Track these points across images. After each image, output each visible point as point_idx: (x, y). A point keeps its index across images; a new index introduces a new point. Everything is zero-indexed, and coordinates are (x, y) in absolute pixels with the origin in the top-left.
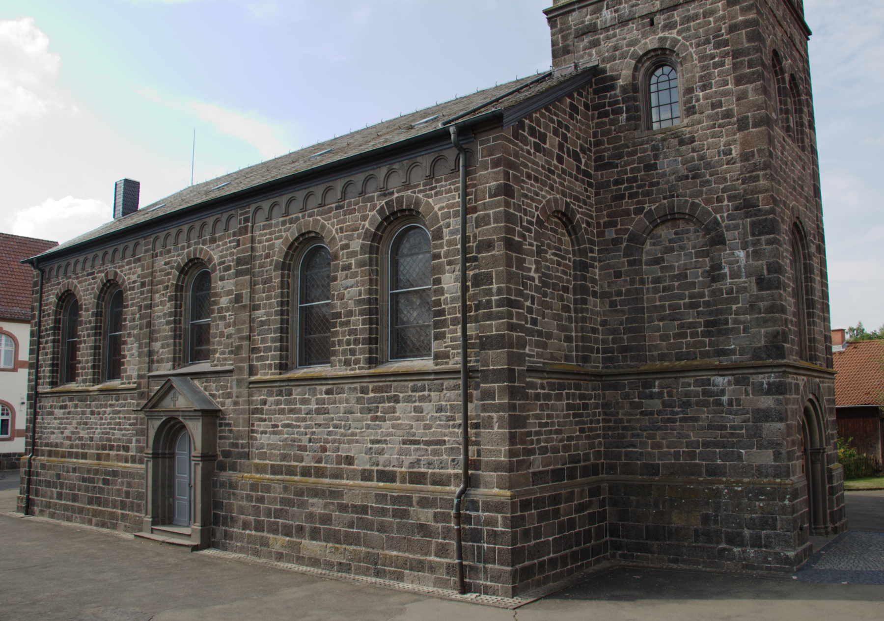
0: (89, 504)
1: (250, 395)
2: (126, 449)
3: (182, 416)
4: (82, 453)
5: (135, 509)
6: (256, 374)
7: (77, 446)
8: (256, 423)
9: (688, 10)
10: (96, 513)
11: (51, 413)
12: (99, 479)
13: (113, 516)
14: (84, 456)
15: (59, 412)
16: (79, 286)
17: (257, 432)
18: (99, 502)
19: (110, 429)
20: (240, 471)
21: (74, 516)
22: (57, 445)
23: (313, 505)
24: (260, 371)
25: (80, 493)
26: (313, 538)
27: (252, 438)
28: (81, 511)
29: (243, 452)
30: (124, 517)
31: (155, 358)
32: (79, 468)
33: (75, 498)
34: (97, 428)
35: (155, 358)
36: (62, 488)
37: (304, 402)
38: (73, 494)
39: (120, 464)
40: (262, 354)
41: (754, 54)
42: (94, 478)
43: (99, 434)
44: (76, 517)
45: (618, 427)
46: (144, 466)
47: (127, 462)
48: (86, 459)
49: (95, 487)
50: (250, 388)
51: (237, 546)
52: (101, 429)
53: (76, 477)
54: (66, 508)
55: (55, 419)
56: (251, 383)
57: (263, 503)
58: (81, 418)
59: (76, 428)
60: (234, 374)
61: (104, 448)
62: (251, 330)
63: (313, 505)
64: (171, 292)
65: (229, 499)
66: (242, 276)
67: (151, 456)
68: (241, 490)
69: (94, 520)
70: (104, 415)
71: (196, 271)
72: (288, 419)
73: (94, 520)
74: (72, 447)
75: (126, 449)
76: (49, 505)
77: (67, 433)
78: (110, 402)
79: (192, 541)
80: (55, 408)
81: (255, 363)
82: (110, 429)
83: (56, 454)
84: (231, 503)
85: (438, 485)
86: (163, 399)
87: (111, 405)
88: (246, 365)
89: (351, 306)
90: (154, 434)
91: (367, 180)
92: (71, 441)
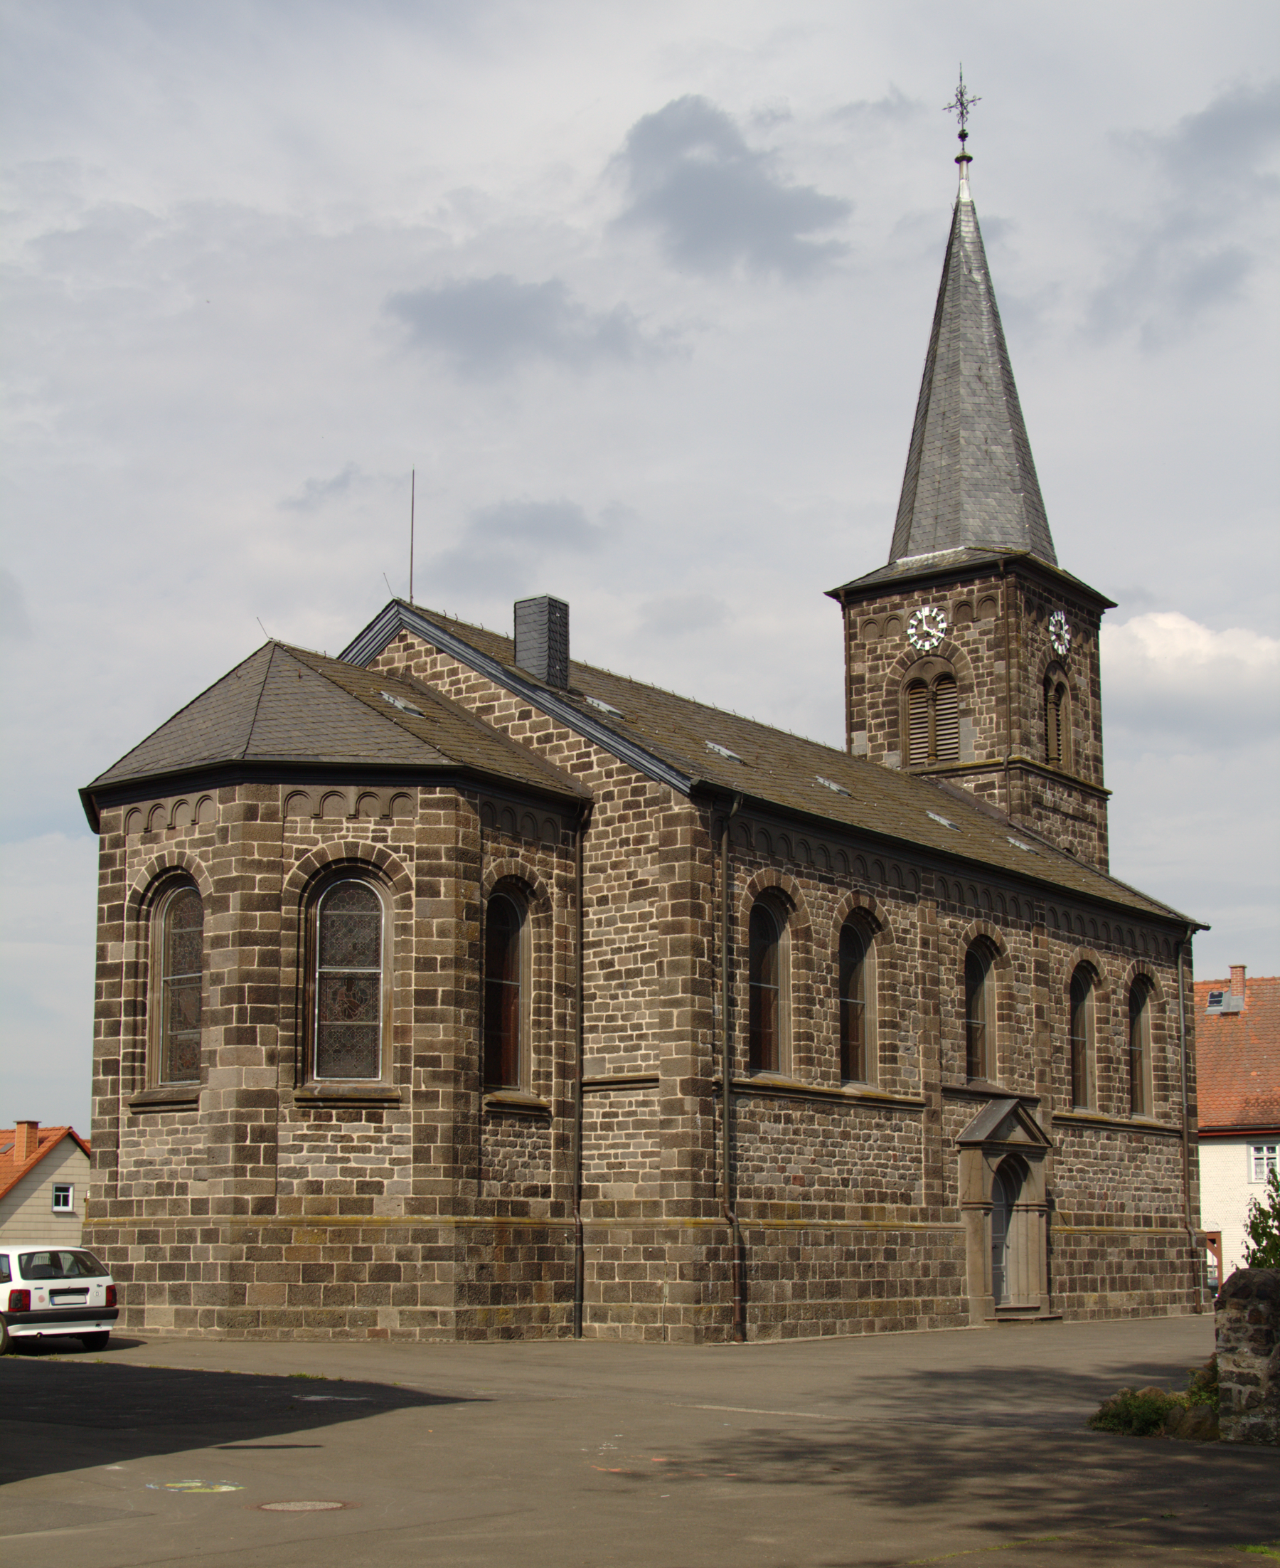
0: (861, 1296)
2: (906, 1199)
4: (835, 1208)
5: (938, 1291)
7: (818, 1196)
10: (881, 1310)
11: (754, 1130)
12: (877, 1251)
13: (910, 1308)
14: (839, 1213)
15: (772, 1129)
16: (801, 891)
18: (879, 1288)
19: (879, 1165)
21: (838, 1322)
22: (770, 1194)
23: (1111, 1254)
25: (842, 1280)
26: (1113, 1289)
28: (850, 1311)
30: (927, 1306)
32: (839, 1234)
33: (833, 1290)
34: (855, 1164)
36: (803, 1275)
37: (1092, 1145)
38: (828, 1284)
39: (905, 1223)
42: (868, 1250)
43: (859, 1173)
44: (843, 1324)
45: (151, 1135)
47: (914, 1219)
48: (843, 1218)
49: (871, 1266)
52: (863, 1165)
53: (834, 1251)
54: (819, 1312)
55: (763, 1140)
57: (618, 1259)
58: (823, 1144)
59: (813, 1162)
61: (869, 1197)
63: (1111, 1254)
64: (960, 969)
69: (878, 1322)
70: (865, 1141)
72: (1080, 1163)
73: (878, 1322)
74: (806, 1197)
75: (906, 1199)
76: (781, 1314)
77: (794, 1169)
78: (877, 1120)
80: (762, 1120)
82: (879, 1165)
83: (778, 1211)
85: (425, 1213)
87: (878, 1126)
89: (1119, 1053)
91: (327, 796)
92: (803, 1186)
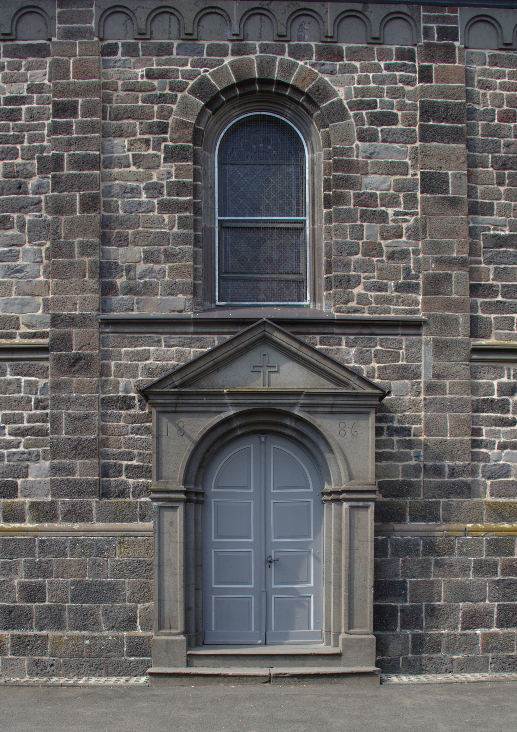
1: (474, 375)
3: (303, 405)
6: (487, 336)
8: (484, 429)
9: (260, 4)
17: (489, 445)
20: (446, 520)
24: (494, 331)
27: (475, 457)
29: (454, 483)
31: (120, 281)
35: (120, 281)
40: (500, 298)
41: (139, 128)
46: (149, 525)
50: (472, 361)
51: (452, 660)
56: (476, 350)
60: (424, 330)
62: (473, 251)
65: (425, 571)
66: (442, 141)
67: (183, 496)
68: (461, 554)
71: (234, 112)
79: (345, 666)
81: (480, 314)
84: (432, 582)
86: (218, 370)
88: (462, 317)
90: (185, 456)
